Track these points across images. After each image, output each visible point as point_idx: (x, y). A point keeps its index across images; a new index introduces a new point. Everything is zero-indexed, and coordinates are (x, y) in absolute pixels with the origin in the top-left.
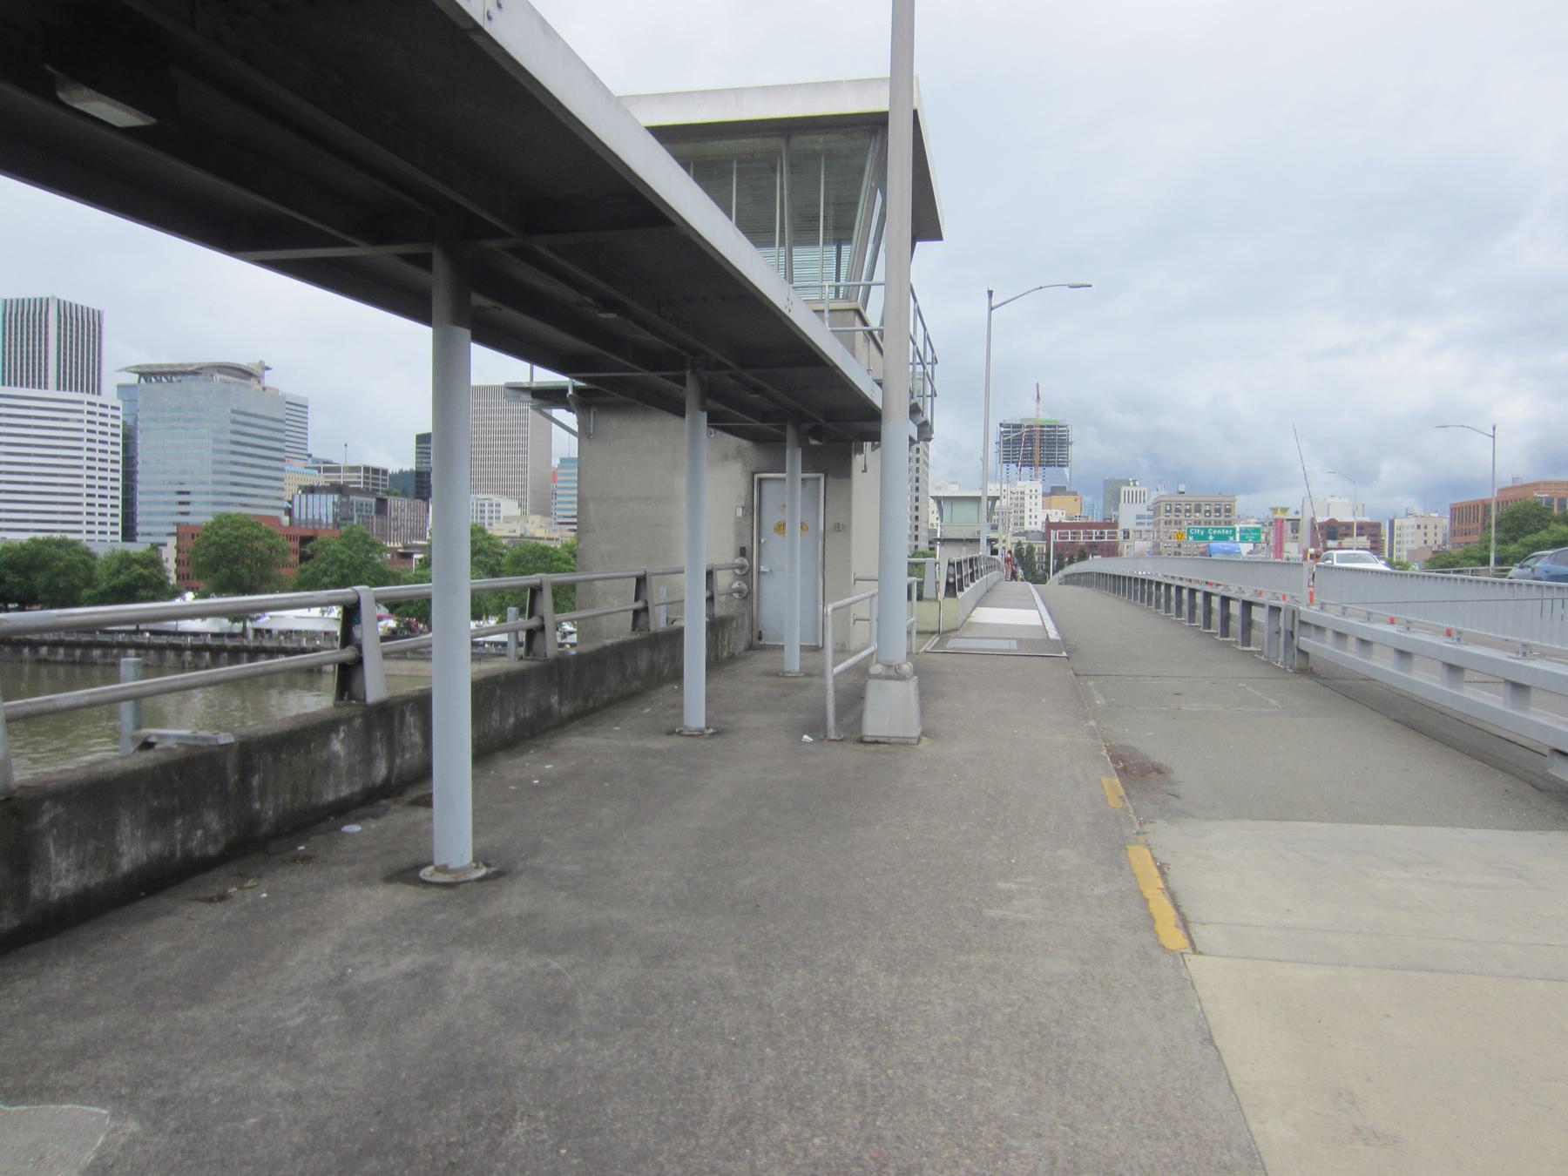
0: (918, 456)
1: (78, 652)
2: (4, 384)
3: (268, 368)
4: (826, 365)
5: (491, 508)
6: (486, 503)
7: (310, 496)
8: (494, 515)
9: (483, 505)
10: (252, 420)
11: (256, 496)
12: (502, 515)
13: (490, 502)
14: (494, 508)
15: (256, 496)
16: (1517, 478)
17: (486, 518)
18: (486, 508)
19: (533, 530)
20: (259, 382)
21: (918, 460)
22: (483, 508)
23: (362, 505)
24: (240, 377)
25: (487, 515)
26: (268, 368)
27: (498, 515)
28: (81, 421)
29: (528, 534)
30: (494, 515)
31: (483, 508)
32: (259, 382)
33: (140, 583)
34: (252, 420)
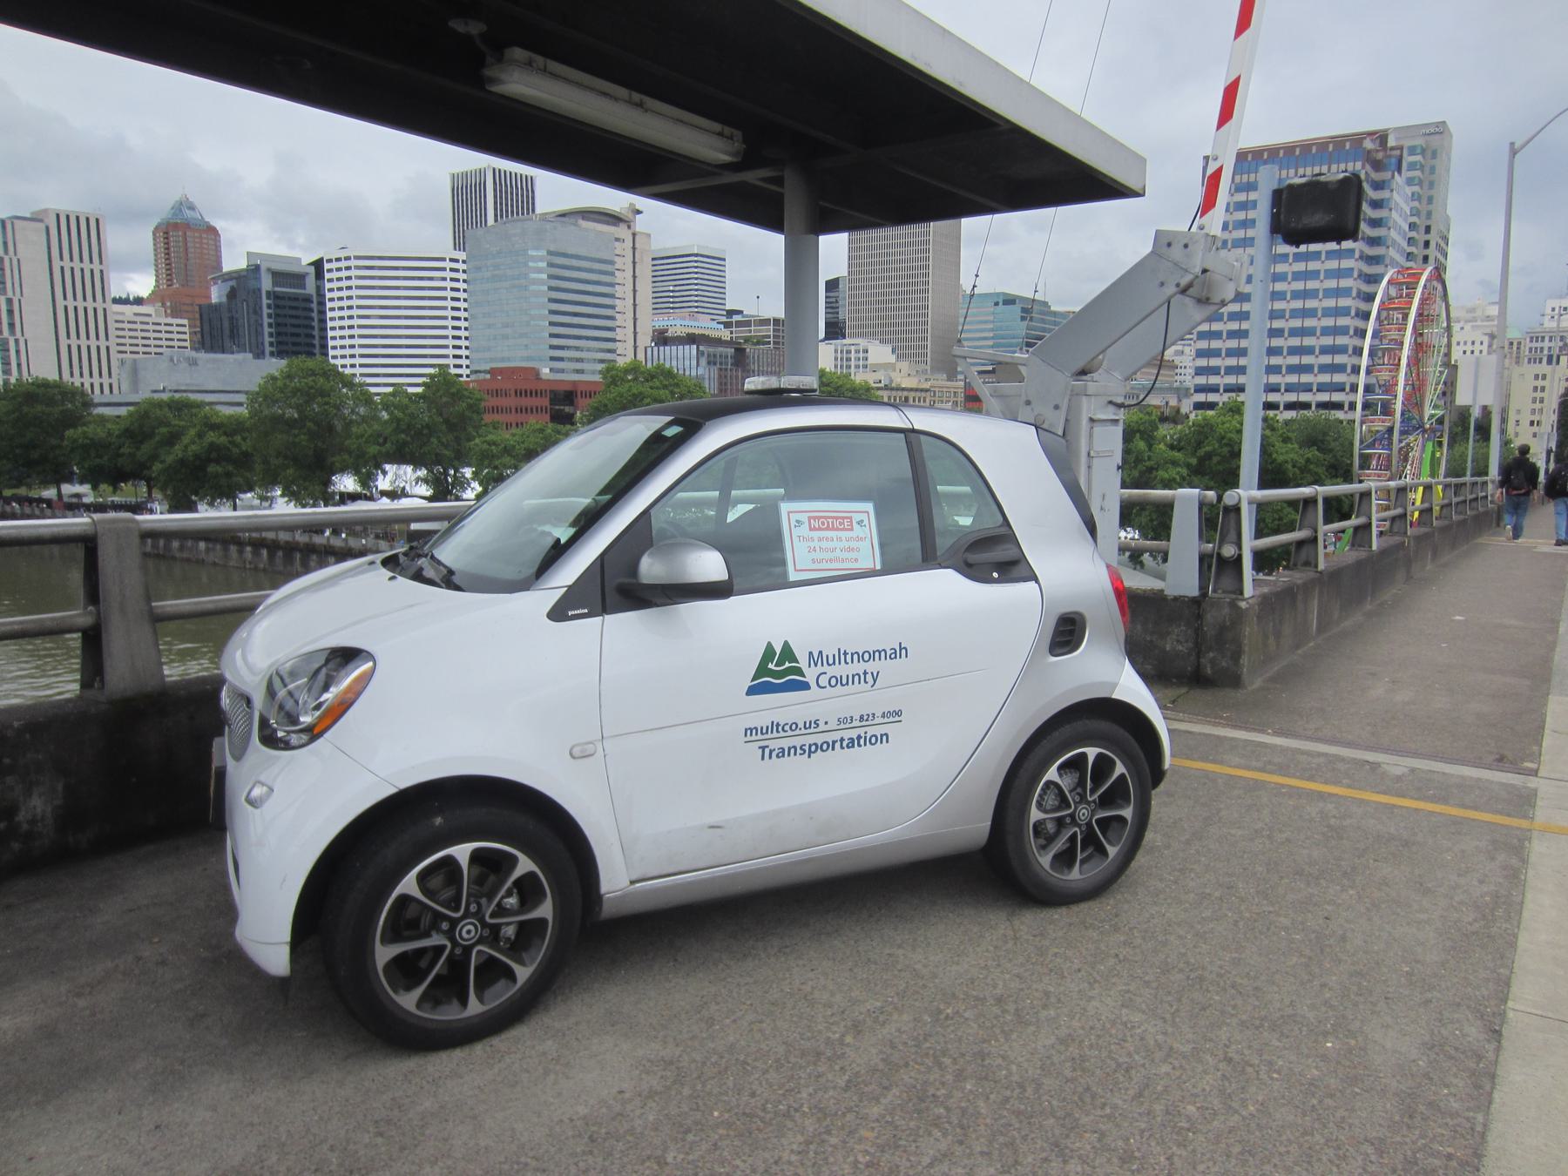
0: (1427, 237)
1: (189, 543)
2: (455, 249)
3: (639, 212)
4: (997, 125)
5: (857, 355)
6: (853, 348)
7: (662, 348)
8: (861, 363)
9: (849, 352)
10: (574, 263)
11: (568, 348)
12: (869, 362)
13: (857, 347)
14: (861, 355)
15: (568, 348)
16: (192, 208)
17: (853, 367)
18: (853, 356)
19: (899, 380)
20: (629, 227)
21: (1427, 244)
22: (849, 355)
23: (715, 356)
24: (608, 223)
25: (853, 363)
26: (639, 212)
27: (865, 363)
28: (444, 279)
29: (894, 385)
30: (861, 363)
31: (849, 355)
32: (629, 227)
33: (214, 455)
34: (574, 263)
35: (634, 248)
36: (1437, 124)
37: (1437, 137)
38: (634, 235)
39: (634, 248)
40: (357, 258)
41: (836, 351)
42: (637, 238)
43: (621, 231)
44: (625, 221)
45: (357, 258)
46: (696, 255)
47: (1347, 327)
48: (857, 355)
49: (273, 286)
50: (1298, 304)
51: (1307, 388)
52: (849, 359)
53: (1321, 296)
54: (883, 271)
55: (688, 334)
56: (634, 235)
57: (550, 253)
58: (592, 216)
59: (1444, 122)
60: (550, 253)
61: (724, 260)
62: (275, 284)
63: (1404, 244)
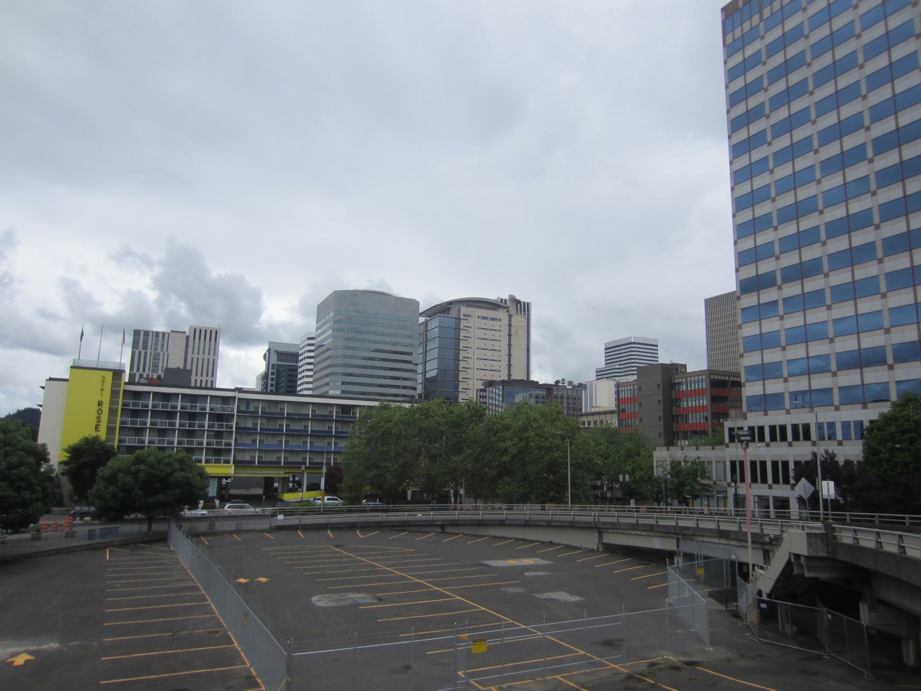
24: (488, 309)
35: (510, 325)
39: (510, 325)
44: (506, 308)
61: (657, 346)
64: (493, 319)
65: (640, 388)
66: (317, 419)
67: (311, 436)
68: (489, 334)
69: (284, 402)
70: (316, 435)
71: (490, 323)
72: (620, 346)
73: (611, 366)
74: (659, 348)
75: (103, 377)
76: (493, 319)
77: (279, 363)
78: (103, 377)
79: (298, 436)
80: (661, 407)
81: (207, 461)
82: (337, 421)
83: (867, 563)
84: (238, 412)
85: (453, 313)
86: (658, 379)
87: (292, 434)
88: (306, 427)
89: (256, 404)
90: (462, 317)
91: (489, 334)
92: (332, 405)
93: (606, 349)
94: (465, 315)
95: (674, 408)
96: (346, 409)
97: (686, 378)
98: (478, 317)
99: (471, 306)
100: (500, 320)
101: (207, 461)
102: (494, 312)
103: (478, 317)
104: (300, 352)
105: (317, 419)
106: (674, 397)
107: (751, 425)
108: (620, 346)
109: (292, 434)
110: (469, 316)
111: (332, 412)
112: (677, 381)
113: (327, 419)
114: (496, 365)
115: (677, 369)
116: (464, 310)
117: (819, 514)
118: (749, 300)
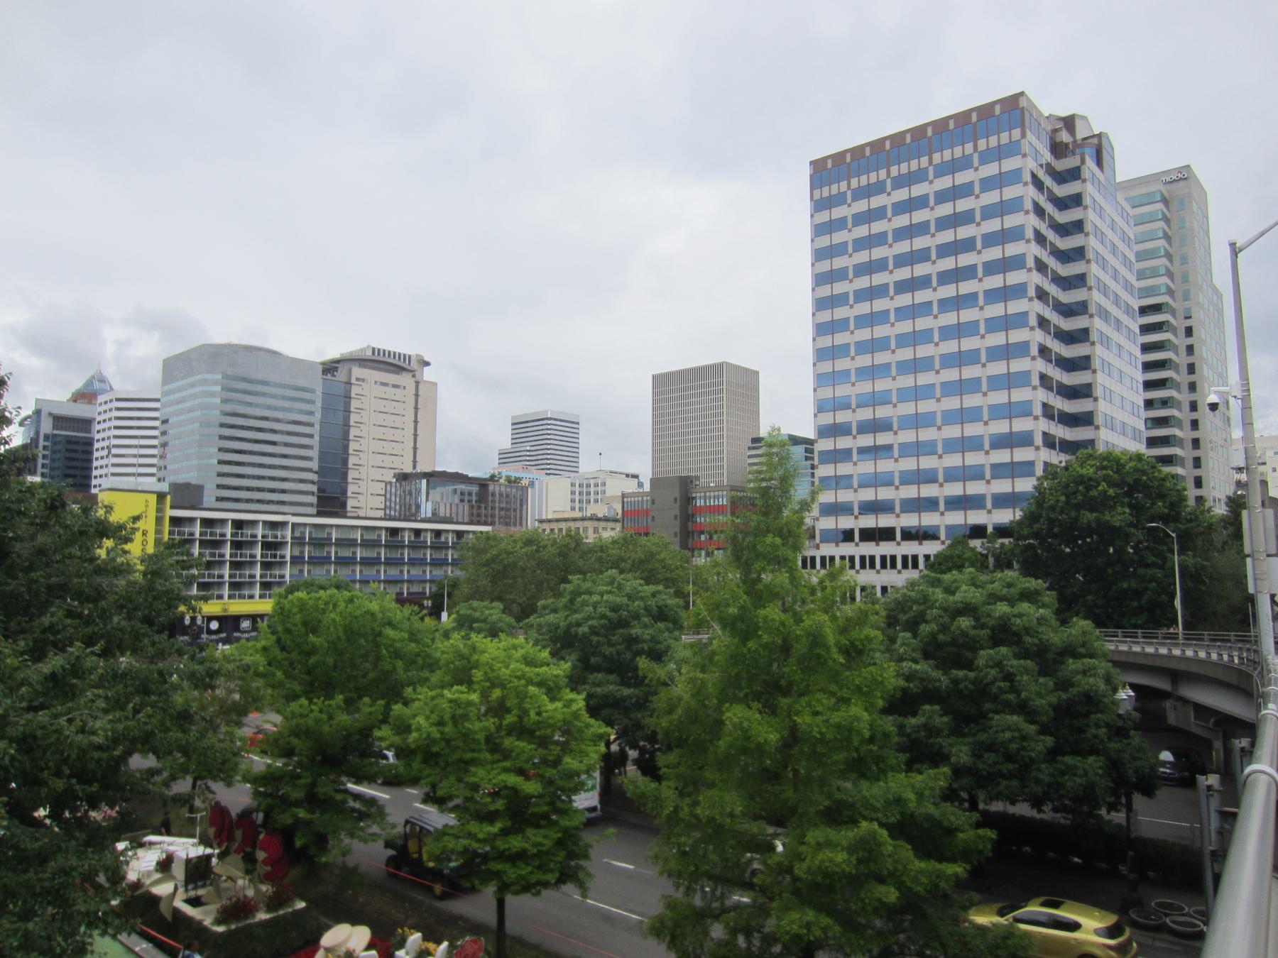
3: (427, 364)
5: (596, 489)
9: (588, 486)
12: (608, 494)
13: (596, 481)
18: (592, 489)
24: (389, 371)
26: (427, 364)
32: (414, 376)
35: (417, 395)
36: (1179, 170)
37: (1182, 184)
38: (417, 383)
39: (417, 395)
40: (118, 400)
41: (573, 485)
42: (421, 387)
43: (404, 379)
44: (411, 371)
45: (118, 400)
46: (551, 419)
47: (1027, 374)
48: (596, 489)
49: (53, 428)
50: (950, 347)
51: (976, 474)
52: (588, 494)
53: (982, 331)
54: (685, 419)
55: (1251, 599)
56: (417, 383)
57: (226, 377)
58: (369, 364)
59: (1188, 166)
60: (226, 377)
61: (578, 423)
62: (55, 427)
63: (1132, 279)
64: (395, 386)
65: (653, 502)
66: (366, 544)
67: (361, 564)
68: (389, 407)
69: (331, 526)
70: (366, 562)
71: (390, 391)
72: (527, 422)
73: (519, 447)
74: (580, 426)
75: (147, 501)
76: (395, 386)
77: (55, 432)
78: (147, 501)
79: (322, 564)
80: (678, 523)
81: (230, 597)
82: (386, 546)
83: (605, 695)
84: (292, 538)
85: (341, 375)
86: (676, 492)
87: (342, 562)
88: (354, 553)
89: (301, 529)
90: (353, 381)
91: (389, 407)
92: (380, 528)
93: (513, 424)
94: (358, 379)
95: (690, 524)
96: (394, 532)
97: (705, 493)
98: (376, 382)
99: (365, 367)
100: (405, 388)
101: (230, 597)
102: (395, 376)
103: (376, 382)
104: (99, 418)
105: (366, 544)
106: (690, 512)
107: (823, 554)
108: (527, 422)
109: (342, 562)
110: (363, 380)
111: (379, 536)
112: (694, 495)
113: (375, 544)
114: (397, 448)
115: (692, 482)
116: (357, 372)
117: (1250, 636)
118: (825, 445)
